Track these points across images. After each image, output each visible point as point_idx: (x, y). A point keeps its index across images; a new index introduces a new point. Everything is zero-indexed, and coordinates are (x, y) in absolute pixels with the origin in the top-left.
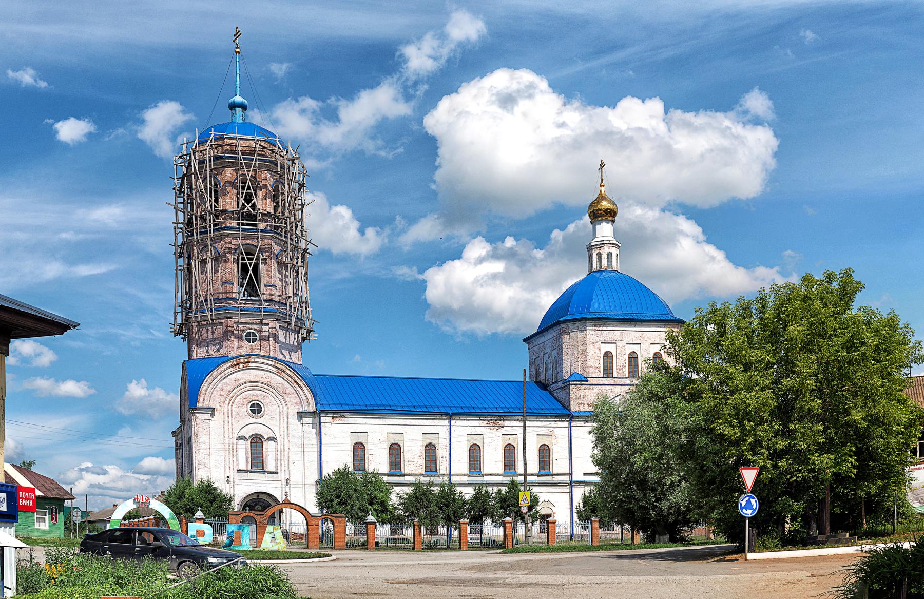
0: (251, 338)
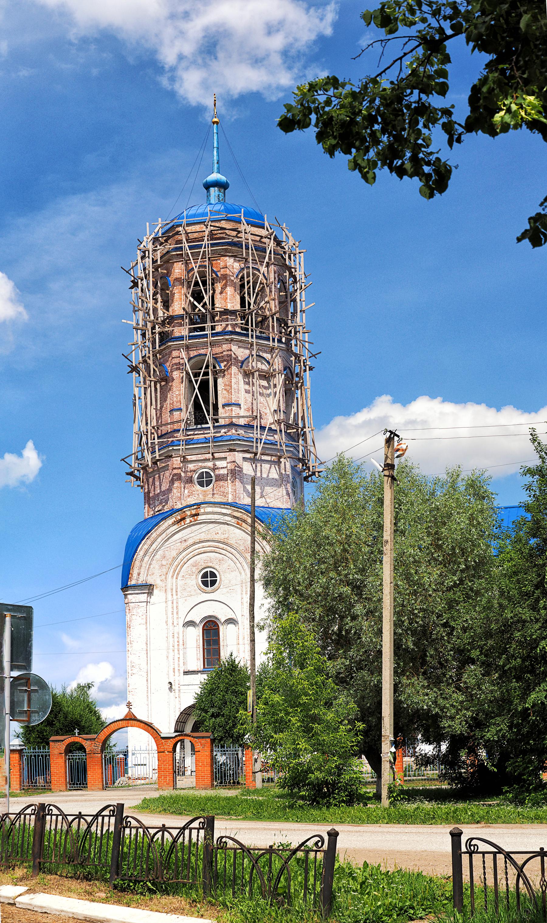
0: (205, 480)
